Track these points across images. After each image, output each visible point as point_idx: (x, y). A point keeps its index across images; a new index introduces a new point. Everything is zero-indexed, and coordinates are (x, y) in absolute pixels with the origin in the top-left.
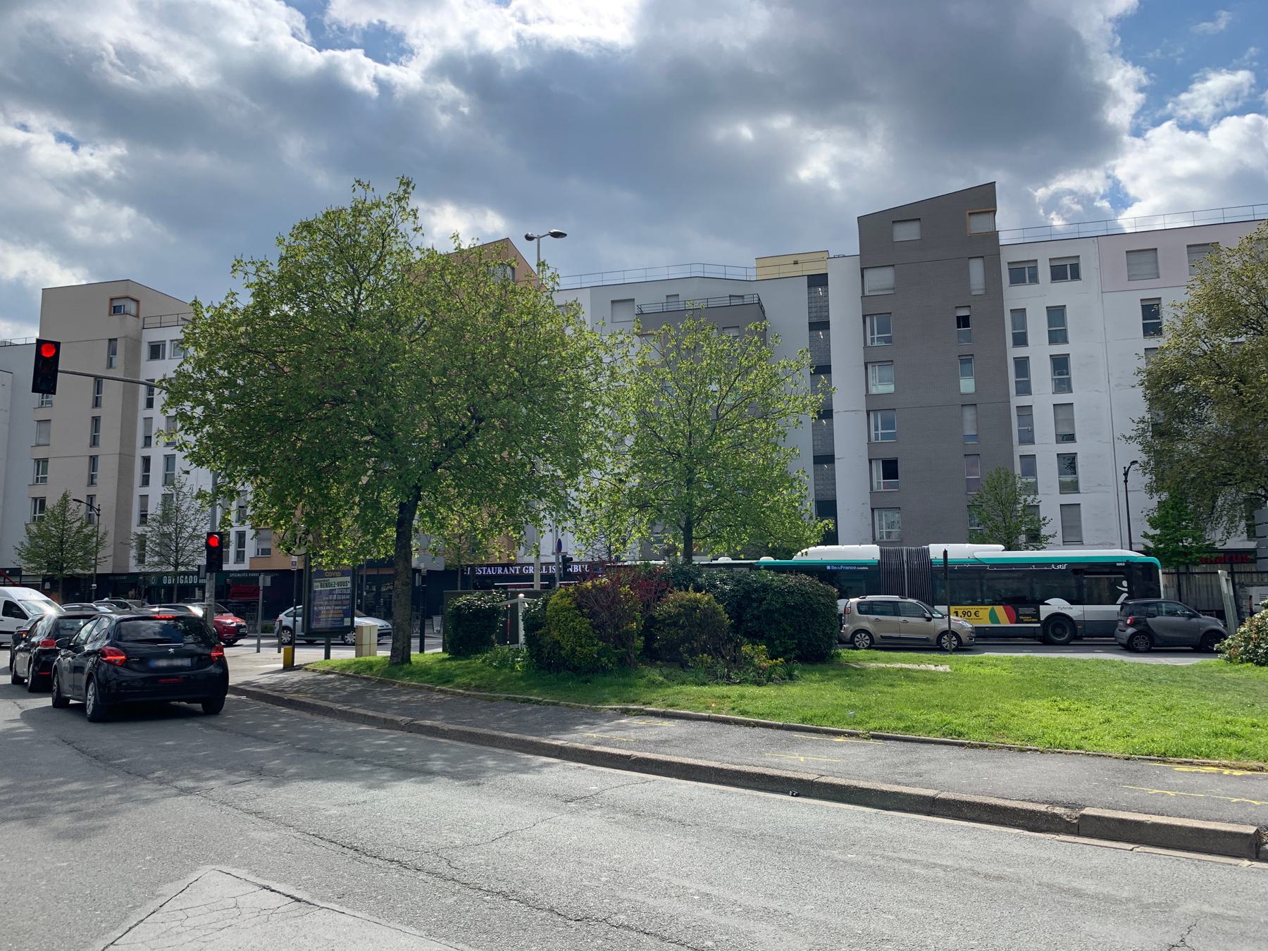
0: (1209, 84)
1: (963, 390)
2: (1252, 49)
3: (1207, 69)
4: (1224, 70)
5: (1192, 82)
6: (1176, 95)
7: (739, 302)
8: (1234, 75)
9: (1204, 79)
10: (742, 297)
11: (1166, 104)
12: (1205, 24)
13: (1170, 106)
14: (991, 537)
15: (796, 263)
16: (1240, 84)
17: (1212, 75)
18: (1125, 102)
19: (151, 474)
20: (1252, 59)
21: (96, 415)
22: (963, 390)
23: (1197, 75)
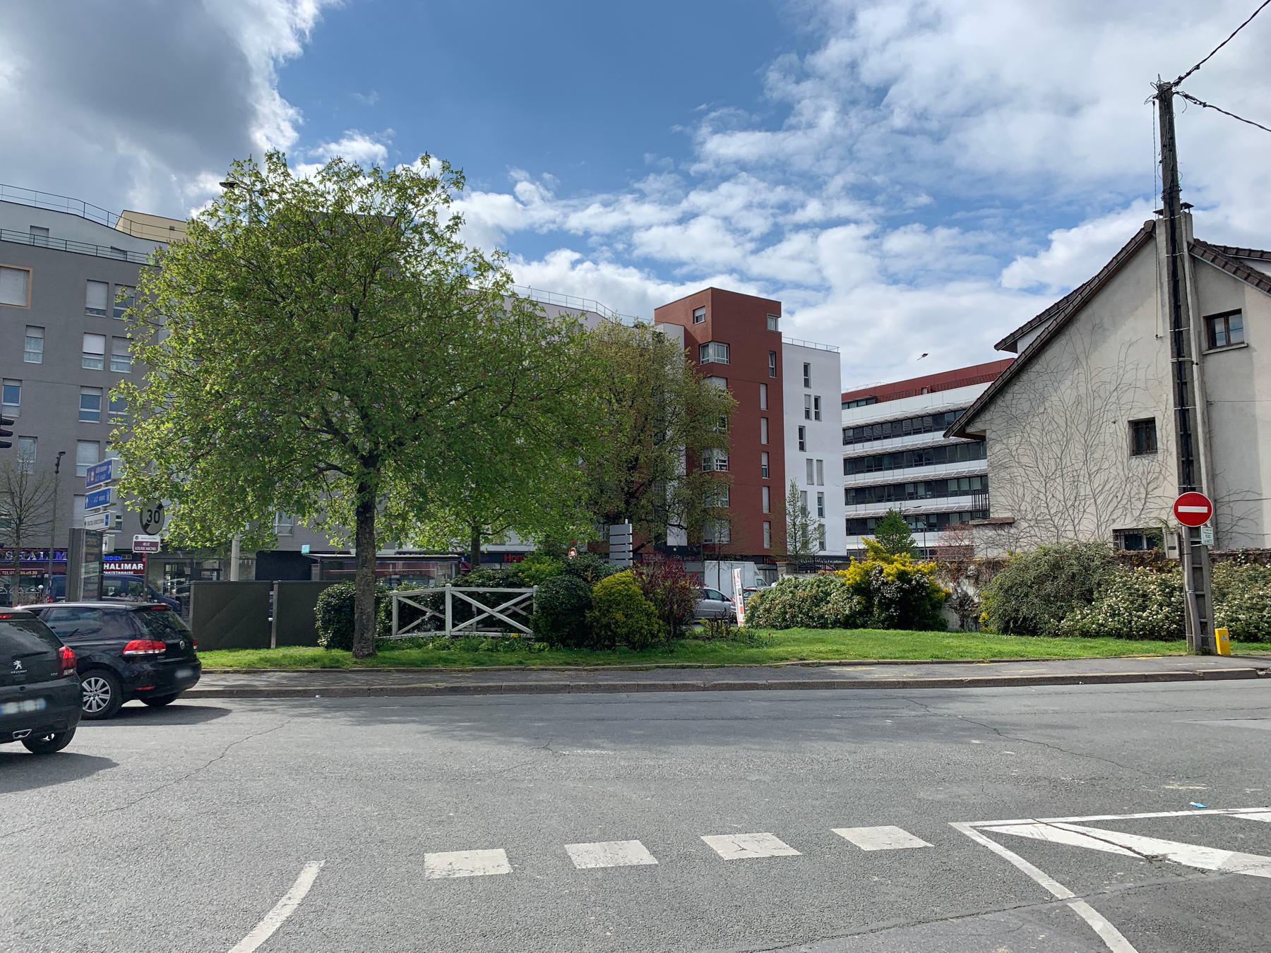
0: (354, 144)
1: (303, 546)
2: (390, 130)
3: (356, 131)
4: (367, 138)
5: (343, 137)
6: (328, 143)
7: (120, 256)
8: (374, 145)
9: (351, 138)
10: (124, 252)
11: (319, 147)
12: (359, 95)
13: (321, 150)
14: (1140, 804)
15: (172, 229)
16: (376, 155)
17: (358, 138)
18: (828, 295)
19: (798, 440)
20: (389, 137)
21: (807, 389)
22: (303, 546)
23: (347, 132)
